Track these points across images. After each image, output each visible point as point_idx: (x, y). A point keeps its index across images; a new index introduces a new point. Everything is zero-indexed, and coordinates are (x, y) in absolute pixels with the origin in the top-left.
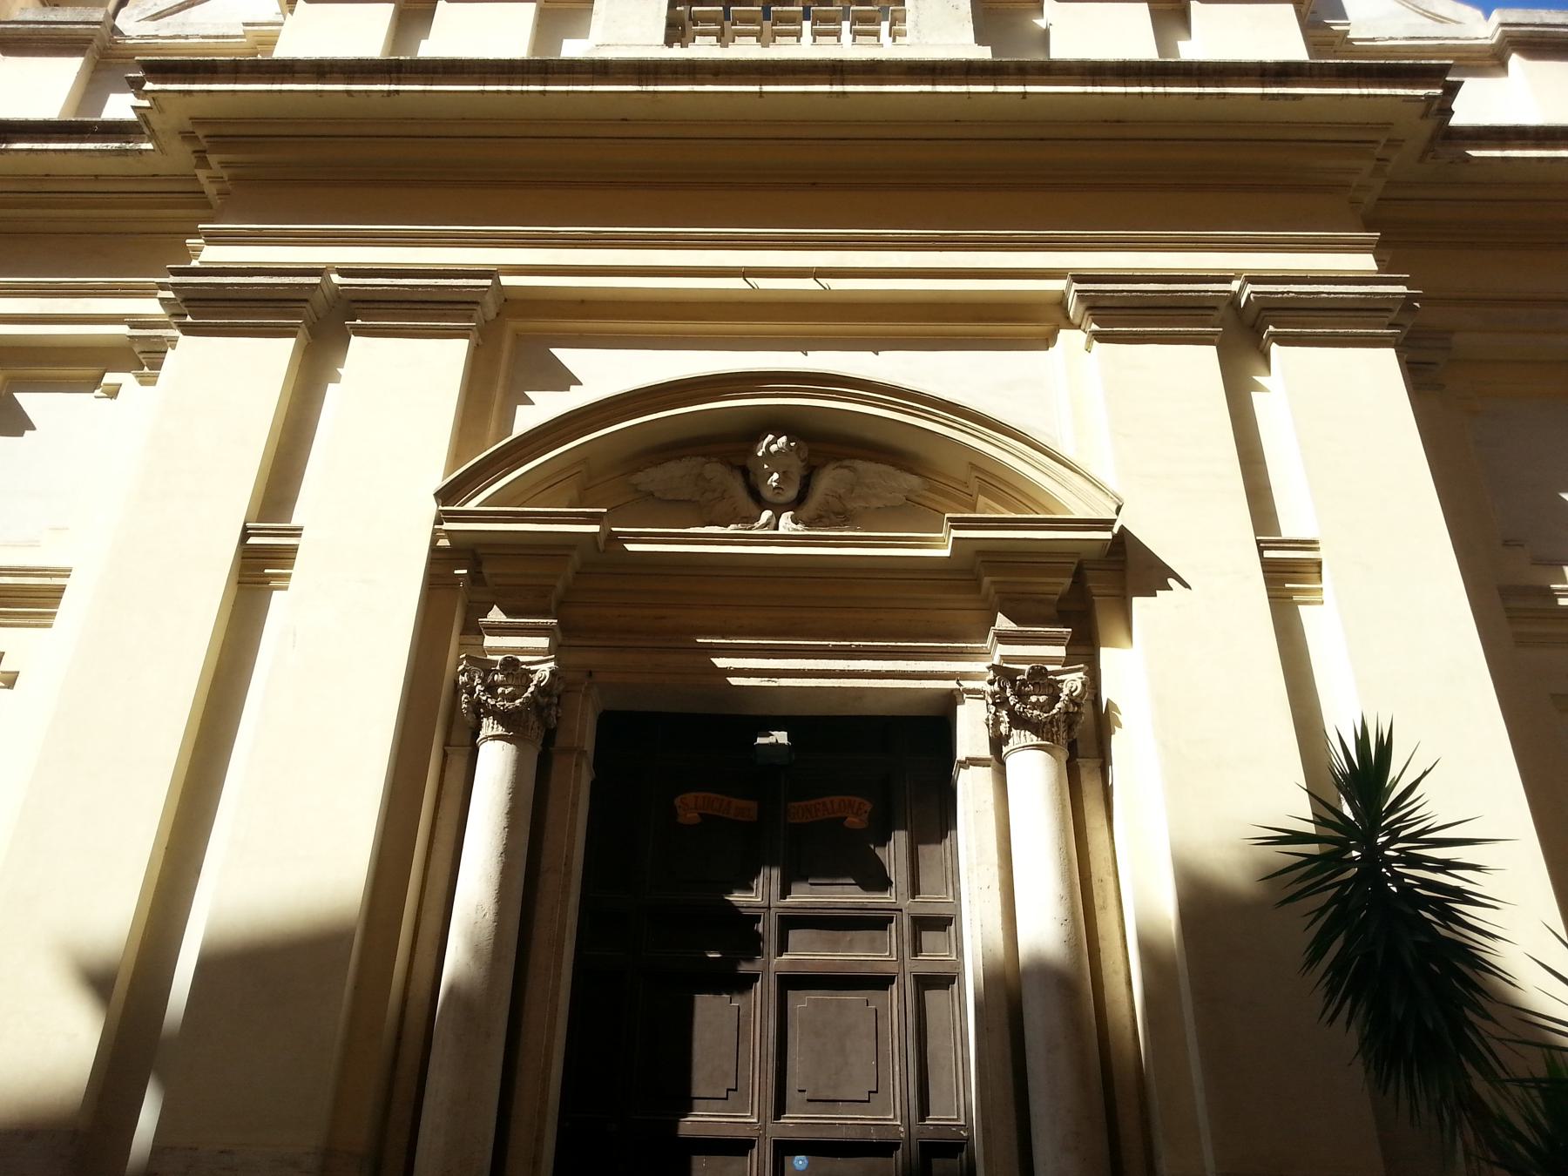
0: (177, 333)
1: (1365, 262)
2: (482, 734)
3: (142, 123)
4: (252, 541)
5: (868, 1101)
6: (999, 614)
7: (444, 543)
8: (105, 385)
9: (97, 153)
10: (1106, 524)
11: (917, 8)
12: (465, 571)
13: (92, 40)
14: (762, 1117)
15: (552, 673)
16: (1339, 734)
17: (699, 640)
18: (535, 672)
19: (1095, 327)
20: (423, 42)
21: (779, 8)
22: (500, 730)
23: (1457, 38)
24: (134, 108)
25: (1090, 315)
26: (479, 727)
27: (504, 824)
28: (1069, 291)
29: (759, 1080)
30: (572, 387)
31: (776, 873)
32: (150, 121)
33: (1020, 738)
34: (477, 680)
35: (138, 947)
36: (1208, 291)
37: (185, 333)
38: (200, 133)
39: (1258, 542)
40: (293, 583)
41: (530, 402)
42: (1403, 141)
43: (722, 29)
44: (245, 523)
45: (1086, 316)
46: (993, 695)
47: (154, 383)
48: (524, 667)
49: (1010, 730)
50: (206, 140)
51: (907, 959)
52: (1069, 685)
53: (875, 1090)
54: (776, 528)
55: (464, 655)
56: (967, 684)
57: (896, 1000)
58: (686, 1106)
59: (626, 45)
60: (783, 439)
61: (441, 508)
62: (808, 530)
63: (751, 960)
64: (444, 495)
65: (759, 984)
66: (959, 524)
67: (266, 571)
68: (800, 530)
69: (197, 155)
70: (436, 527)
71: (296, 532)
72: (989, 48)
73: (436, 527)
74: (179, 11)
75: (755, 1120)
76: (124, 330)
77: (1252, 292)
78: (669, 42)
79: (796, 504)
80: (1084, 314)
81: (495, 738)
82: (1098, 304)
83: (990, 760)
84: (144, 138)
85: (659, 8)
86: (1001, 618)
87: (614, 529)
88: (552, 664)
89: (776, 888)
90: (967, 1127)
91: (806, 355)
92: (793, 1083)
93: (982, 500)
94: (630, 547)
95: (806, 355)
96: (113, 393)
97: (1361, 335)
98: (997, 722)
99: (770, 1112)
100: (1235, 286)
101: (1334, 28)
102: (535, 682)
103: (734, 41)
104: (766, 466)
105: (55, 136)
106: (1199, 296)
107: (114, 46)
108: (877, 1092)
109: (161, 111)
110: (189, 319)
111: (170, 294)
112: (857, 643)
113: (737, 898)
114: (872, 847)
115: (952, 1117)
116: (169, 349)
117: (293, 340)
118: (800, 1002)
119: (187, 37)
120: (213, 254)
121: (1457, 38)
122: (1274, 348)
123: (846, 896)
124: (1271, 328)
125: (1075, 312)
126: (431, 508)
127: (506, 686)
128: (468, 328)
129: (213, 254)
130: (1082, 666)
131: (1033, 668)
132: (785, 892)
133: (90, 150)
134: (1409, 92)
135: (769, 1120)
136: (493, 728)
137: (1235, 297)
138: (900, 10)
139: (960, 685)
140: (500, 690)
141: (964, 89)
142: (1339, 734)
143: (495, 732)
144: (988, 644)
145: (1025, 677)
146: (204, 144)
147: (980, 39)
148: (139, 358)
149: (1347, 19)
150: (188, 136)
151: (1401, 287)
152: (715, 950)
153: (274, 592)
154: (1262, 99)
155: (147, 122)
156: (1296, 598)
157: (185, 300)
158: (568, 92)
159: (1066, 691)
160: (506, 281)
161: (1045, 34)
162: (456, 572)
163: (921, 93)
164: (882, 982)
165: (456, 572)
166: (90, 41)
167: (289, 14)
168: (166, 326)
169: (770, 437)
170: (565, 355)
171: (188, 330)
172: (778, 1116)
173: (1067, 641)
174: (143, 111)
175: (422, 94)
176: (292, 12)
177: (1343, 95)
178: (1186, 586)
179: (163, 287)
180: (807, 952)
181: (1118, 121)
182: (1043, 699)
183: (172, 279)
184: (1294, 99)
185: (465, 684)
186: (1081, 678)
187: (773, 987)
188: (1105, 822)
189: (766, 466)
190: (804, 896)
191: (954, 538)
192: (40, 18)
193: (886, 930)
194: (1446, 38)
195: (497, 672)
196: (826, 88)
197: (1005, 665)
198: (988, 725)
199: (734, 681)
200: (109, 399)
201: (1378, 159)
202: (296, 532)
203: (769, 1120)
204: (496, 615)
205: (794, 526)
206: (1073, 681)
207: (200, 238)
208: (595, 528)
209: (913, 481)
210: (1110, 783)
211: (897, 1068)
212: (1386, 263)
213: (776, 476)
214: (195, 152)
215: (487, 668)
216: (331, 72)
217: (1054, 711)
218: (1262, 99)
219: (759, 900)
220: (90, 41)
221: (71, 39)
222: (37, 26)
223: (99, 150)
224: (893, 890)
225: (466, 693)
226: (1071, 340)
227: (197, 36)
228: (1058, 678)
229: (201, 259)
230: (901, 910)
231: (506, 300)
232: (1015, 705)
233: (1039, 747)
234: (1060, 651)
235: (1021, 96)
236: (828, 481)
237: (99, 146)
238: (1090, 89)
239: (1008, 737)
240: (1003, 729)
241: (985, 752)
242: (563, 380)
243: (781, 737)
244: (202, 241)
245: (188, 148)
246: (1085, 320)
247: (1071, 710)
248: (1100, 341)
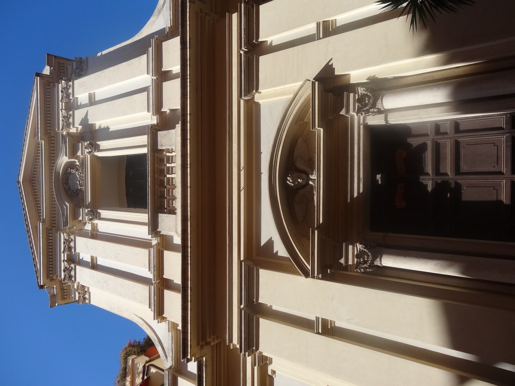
0: (258, 352)
1: (235, 16)
2: (379, 265)
3: (198, 360)
4: (320, 331)
5: (497, 146)
6: (340, 113)
7: (320, 276)
8: (272, 374)
9: (206, 373)
10: (313, 84)
11: (165, 146)
12: (329, 270)
13: (173, 375)
14: (503, 178)
15: (360, 244)
16: (381, 8)
17: (349, 202)
18: (360, 249)
19: (254, 91)
20: (175, 282)
21: (165, 183)
22: (378, 259)
24: (195, 361)
25: (251, 93)
26: (377, 266)
27: (408, 258)
28: (244, 99)
29: (491, 180)
30: (273, 240)
31: (421, 177)
32: (198, 357)
33: (379, 105)
34: (363, 266)
35: (450, 369)
36: (244, 60)
37: (258, 349)
38: (201, 343)
39: (318, 40)
41: (277, 252)
42: (200, 8)
43: (171, 199)
44: (315, 333)
45: (251, 94)
46: (365, 114)
47: (272, 359)
48: (358, 253)
49: (376, 108)
50: (203, 342)
51: (449, 136)
52: (362, 91)
53: (494, 144)
54: (315, 180)
55: (355, 270)
56: (362, 122)
57: (463, 139)
58: (501, 202)
59: (176, 225)
60: (288, 178)
61: (310, 276)
62: (315, 170)
63: (450, 184)
64: (306, 274)
65: (458, 181)
66: (314, 126)
67: (329, 327)
68: (315, 173)
69: (207, 345)
70: (315, 278)
71: (317, 318)
72: (176, 125)
73: (315, 278)
74: (165, 351)
75: (504, 181)
76: (256, 368)
77: (244, 47)
78: (175, 213)
79: (307, 174)
80: (251, 95)
81: (381, 261)
82: (248, 91)
83: (385, 114)
84: (202, 360)
85: (166, 216)
86: (341, 113)
87: (316, 227)
88: (358, 244)
89: (427, 177)
90: (506, 115)
91: (262, 173)
92: (492, 169)
93: (305, 120)
94: (321, 221)
95: (262, 173)
96: (274, 372)
97: (256, 16)
98: (373, 112)
99: (502, 176)
100: (242, 52)
101: (168, 31)
102: (363, 249)
103: (175, 196)
104: (296, 183)
105: (201, 384)
106: (245, 62)
107: (175, 368)
108: (494, 143)
109: (195, 354)
110: (254, 348)
111: (247, 353)
112: (349, 155)
113: (430, 189)
114: (413, 148)
115: (503, 120)
116: (262, 354)
117: (260, 319)
118: (464, 168)
119: (172, 348)
120: (235, 341)
122: (260, 40)
123: (429, 156)
124: (254, 41)
125: (250, 97)
126: (309, 279)
127: (364, 258)
129: (235, 341)
130: (356, 88)
131: (357, 102)
132: (428, 174)
133: (205, 375)
134: (188, 8)
135: (504, 176)
136: (377, 262)
137: (245, 52)
138: (166, 151)
139: (362, 124)
140: (366, 259)
141: (189, 131)
142: (381, 8)
143: (379, 261)
144: (349, 116)
145: (360, 104)
146: (204, 342)
147: (174, 128)
148: (264, 364)
149: (165, 28)
150: (202, 347)
151: (242, 5)
152: (447, 195)
153: (336, 325)
154: (191, 48)
155: (198, 358)
156: (334, 27)
157: (249, 349)
158: (190, 241)
159: (364, 92)
160: (242, 258)
161: (172, 111)
162: (329, 272)
163: (190, 143)
164: (457, 145)
165: (329, 272)
166: (174, 375)
167: (167, 319)
168: (255, 356)
169: (288, 182)
170: (263, 242)
171: (257, 348)
172: (503, 174)
173: (348, 93)
174: (195, 359)
175: (191, 281)
176: (166, 318)
178: (331, 59)
179: (245, 355)
180: (448, 167)
181: (197, 88)
182: (367, 99)
183: (243, 352)
184: (190, 39)
185: (364, 270)
186: (360, 88)
187: (459, 177)
188: (405, 78)
189: (296, 183)
190: (429, 168)
191: (318, 127)
193: (440, 143)
195: (360, 260)
196: (189, 169)
197: (356, 111)
198: (374, 115)
199: (361, 191)
200: (276, 373)
201: (206, 15)
202: (317, 318)
203: (504, 176)
204: (342, 261)
205: (314, 174)
206: (361, 90)
207: (230, 344)
208: (316, 232)
209: (300, 140)
210: (392, 78)
211: (486, 137)
212: (235, 10)
213: (299, 180)
214: (206, 345)
215: (359, 263)
216: (185, 306)
217: (371, 95)
218: (191, 48)
219: (430, 182)
220: (174, 375)
221: (173, 380)
223: (206, 372)
224: (427, 141)
225: (366, 270)
226: (258, 98)
227: (172, 345)
228: (360, 95)
229: (236, 344)
230: (433, 139)
231: (247, 259)
232: (369, 107)
233: (382, 100)
234: (352, 95)
235: (191, 115)
236: (300, 165)
237: (204, 372)
238: (188, 96)
239: (378, 109)
240: (376, 110)
241: (383, 116)
242: (270, 243)
243: (378, 177)
244: (231, 344)
245: (205, 347)
246: (253, 94)
247: (370, 90)
248: (258, 89)
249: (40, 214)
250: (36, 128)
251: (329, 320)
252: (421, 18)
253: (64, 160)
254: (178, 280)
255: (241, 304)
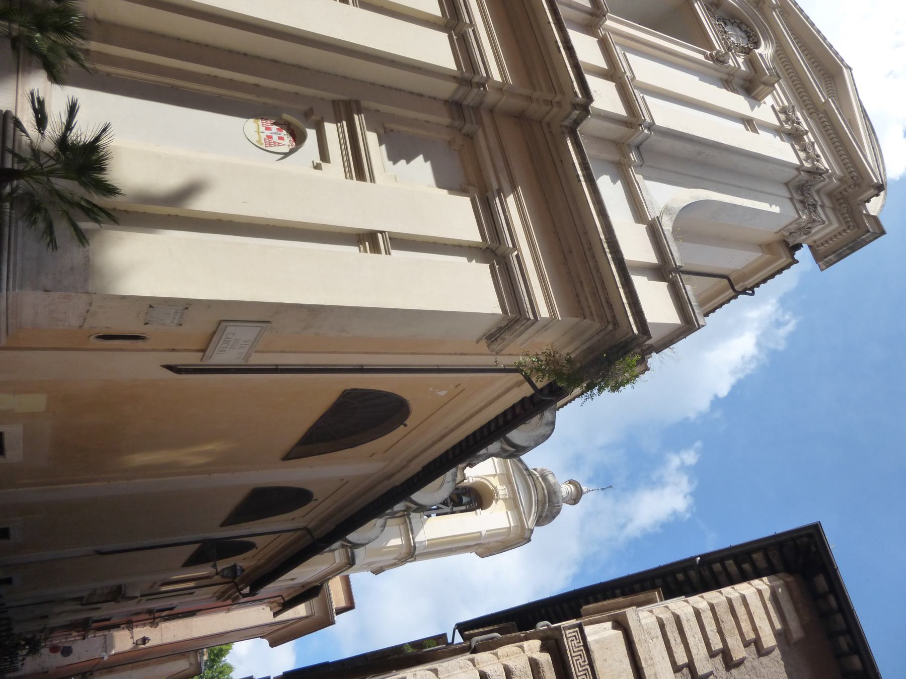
4: (380, 235)
23: (647, 207)
40: (363, 254)
71: (388, 252)
121: (647, 207)
128: (487, 241)
166: (599, 9)
177: (566, 65)
192: (676, 260)
194: (645, 203)
202: (388, 252)
222: (661, 231)
249: (800, 44)
250: (851, 126)
251: (357, 180)
252: (299, 533)
253: (765, 51)
254: (640, 283)
255: (517, 256)
